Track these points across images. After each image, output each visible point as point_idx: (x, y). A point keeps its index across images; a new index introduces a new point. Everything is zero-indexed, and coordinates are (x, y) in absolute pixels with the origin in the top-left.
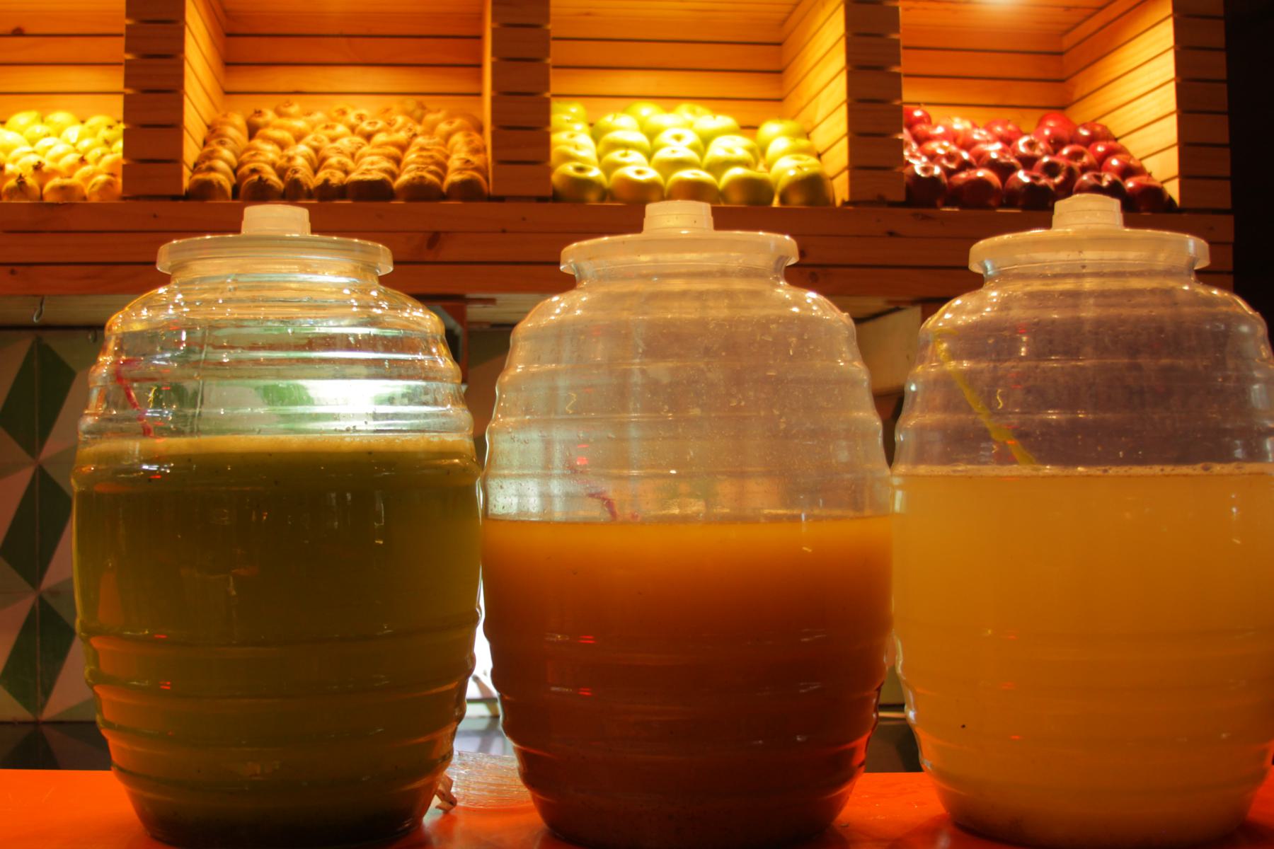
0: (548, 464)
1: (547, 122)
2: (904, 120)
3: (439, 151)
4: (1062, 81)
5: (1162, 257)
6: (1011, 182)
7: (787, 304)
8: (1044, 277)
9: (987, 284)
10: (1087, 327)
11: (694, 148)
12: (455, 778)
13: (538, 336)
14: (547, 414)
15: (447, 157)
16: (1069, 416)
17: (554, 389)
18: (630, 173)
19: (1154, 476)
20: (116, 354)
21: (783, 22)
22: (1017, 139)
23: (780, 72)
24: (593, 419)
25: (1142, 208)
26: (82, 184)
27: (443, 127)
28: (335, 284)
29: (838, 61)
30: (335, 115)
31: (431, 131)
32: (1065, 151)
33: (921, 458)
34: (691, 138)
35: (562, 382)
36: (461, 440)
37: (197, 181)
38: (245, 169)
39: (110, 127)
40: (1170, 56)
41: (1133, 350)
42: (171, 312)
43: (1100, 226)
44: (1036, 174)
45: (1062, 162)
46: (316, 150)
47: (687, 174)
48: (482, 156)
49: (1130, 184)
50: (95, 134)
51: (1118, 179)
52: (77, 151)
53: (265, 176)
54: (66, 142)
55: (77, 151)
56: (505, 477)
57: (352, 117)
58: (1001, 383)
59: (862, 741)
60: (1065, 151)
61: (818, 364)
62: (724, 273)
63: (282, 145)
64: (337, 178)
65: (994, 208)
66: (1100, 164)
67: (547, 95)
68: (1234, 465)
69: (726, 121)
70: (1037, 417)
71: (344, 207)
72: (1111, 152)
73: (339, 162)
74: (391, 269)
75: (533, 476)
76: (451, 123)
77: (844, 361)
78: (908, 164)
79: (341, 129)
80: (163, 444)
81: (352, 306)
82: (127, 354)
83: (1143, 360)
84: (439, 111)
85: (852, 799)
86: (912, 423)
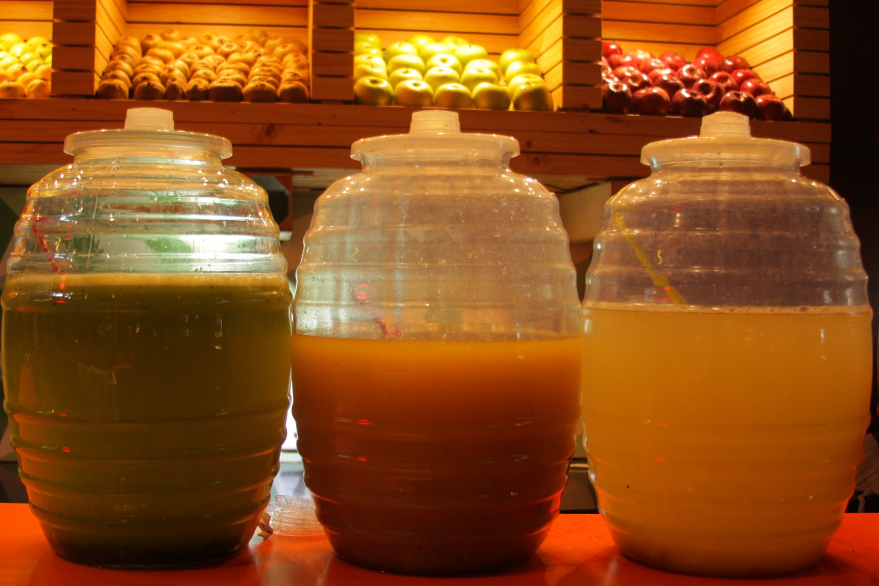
0: (337, 298)
1: (352, 48)
2: (603, 50)
3: (275, 67)
4: (715, 26)
5: (777, 157)
6: (677, 96)
7: (510, 186)
8: (693, 169)
9: (653, 175)
10: (721, 207)
11: (455, 68)
12: (272, 514)
13: (333, 205)
14: (337, 262)
15: (281, 71)
16: (707, 271)
17: (343, 244)
18: (409, 85)
19: (766, 314)
20: (34, 214)
22: (682, 66)
23: (517, 15)
24: (370, 266)
25: (768, 117)
26: (23, 86)
27: (279, 50)
28: (192, 166)
30: (203, 39)
31: (270, 52)
32: (715, 76)
33: (603, 295)
34: (453, 61)
35: (349, 239)
36: (278, 278)
37: (104, 85)
38: (139, 77)
39: (44, 45)
40: (790, 11)
42: (75, 184)
43: (733, 135)
44: (695, 92)
45: (712, 83)
46: (189, 64)
47: (449, 87)
48: (306, 71)
49: (760, 100)
50: (34, 50)
51: (751, 96)
52: (20, 62)
53: (152, 83)
54: (13, 55)
55: (20, 62)
56: (308, 305)
57: (215, 42)
58: (661, 245)
59: (559, 494)
60: (715, 76)
61: (531, 229)
62: (465, 163)
63: (165, 60)
64: (203, 84)
65: (663, 115)
66: (739, 86)
67: (352, 29)
68: (823, 307)
69: (478, 49)
70: (685, 271)
71: (199, 107)
72: (747, 77)
73: (205, 74)
74: (231, 155)
75: (327, 305)
76: (285, 47)
77: (550, 227)
78: (605, 82)
79: (207, 49)
80: (64, 278)
81: (203, 182)
82: (41, 213)
83: (760, 232)
84: (277, 38)
86: (597, 271)
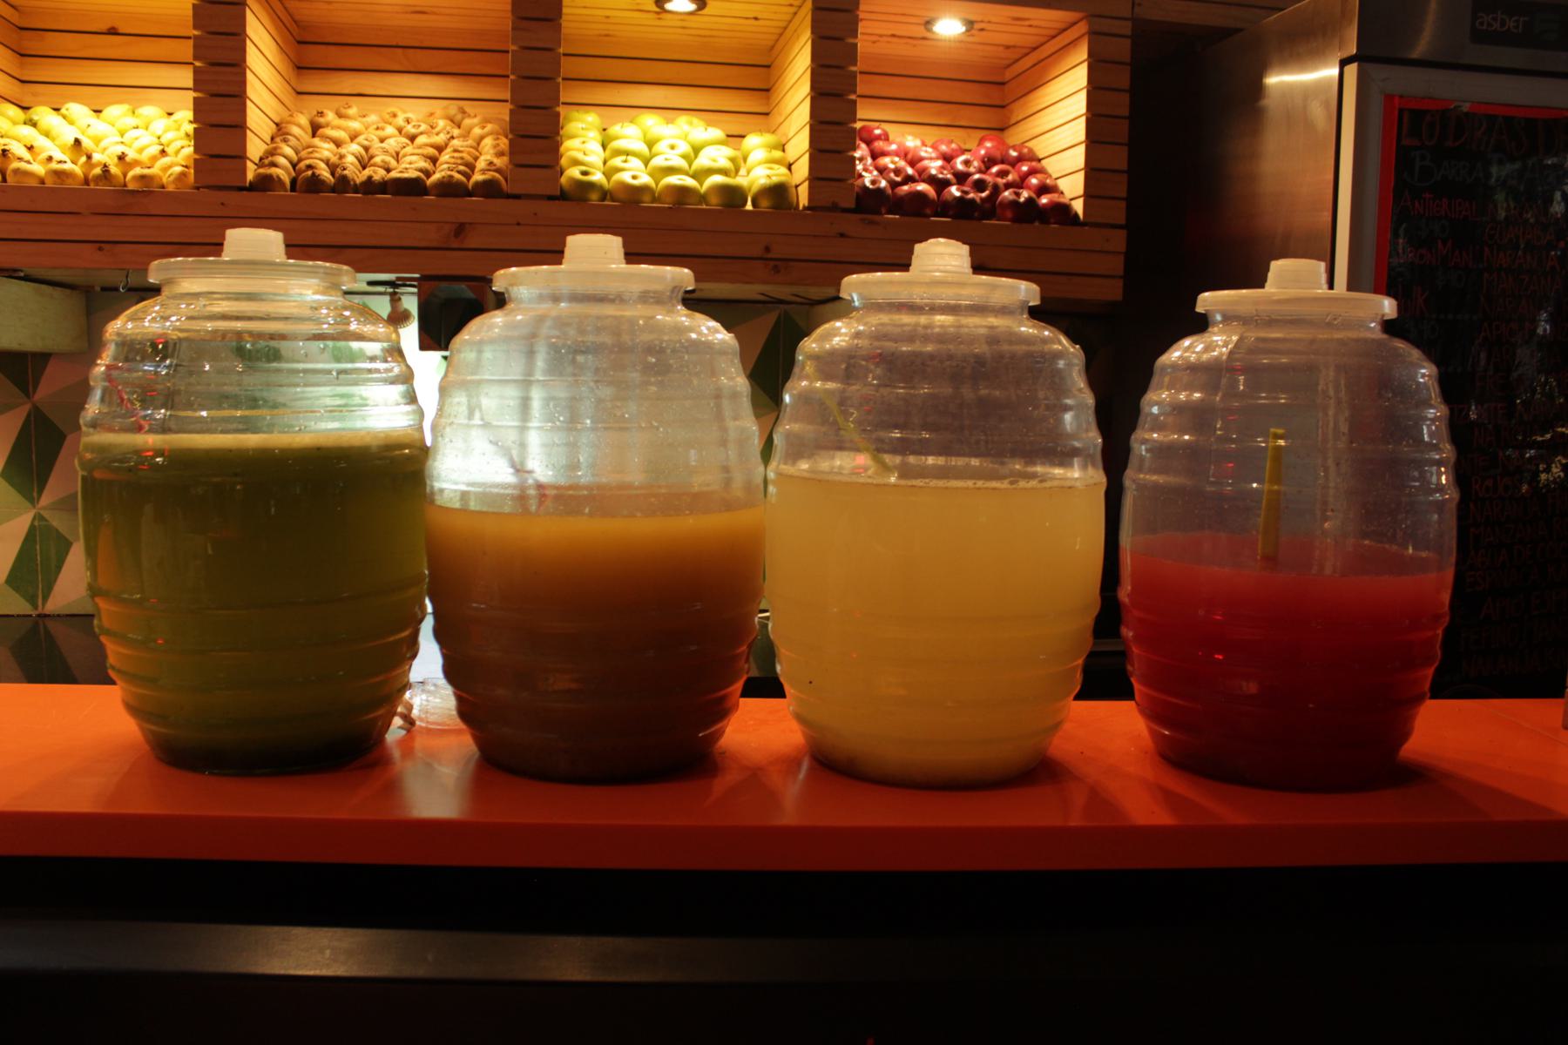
11: (685, 157)
15: (476, 159)
18: (626, 177)
21: (772, 47)
27: (477, 131)
29: (805, 88)
31: (465, 136)
34: (685, 148)
38: (302, 165)
41: (956, 377)
46: (366, 149)
49: (1044, 200)
57: (400, 121)
60: (995, 169)
63: (338, 143)
64: (379, 175)
69: (717, 133)
72: (1033, 172)
78: (861, 176)
79: (390, 130)
85: (728, 730)
